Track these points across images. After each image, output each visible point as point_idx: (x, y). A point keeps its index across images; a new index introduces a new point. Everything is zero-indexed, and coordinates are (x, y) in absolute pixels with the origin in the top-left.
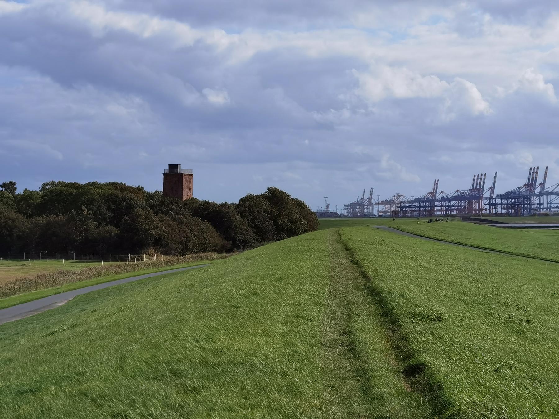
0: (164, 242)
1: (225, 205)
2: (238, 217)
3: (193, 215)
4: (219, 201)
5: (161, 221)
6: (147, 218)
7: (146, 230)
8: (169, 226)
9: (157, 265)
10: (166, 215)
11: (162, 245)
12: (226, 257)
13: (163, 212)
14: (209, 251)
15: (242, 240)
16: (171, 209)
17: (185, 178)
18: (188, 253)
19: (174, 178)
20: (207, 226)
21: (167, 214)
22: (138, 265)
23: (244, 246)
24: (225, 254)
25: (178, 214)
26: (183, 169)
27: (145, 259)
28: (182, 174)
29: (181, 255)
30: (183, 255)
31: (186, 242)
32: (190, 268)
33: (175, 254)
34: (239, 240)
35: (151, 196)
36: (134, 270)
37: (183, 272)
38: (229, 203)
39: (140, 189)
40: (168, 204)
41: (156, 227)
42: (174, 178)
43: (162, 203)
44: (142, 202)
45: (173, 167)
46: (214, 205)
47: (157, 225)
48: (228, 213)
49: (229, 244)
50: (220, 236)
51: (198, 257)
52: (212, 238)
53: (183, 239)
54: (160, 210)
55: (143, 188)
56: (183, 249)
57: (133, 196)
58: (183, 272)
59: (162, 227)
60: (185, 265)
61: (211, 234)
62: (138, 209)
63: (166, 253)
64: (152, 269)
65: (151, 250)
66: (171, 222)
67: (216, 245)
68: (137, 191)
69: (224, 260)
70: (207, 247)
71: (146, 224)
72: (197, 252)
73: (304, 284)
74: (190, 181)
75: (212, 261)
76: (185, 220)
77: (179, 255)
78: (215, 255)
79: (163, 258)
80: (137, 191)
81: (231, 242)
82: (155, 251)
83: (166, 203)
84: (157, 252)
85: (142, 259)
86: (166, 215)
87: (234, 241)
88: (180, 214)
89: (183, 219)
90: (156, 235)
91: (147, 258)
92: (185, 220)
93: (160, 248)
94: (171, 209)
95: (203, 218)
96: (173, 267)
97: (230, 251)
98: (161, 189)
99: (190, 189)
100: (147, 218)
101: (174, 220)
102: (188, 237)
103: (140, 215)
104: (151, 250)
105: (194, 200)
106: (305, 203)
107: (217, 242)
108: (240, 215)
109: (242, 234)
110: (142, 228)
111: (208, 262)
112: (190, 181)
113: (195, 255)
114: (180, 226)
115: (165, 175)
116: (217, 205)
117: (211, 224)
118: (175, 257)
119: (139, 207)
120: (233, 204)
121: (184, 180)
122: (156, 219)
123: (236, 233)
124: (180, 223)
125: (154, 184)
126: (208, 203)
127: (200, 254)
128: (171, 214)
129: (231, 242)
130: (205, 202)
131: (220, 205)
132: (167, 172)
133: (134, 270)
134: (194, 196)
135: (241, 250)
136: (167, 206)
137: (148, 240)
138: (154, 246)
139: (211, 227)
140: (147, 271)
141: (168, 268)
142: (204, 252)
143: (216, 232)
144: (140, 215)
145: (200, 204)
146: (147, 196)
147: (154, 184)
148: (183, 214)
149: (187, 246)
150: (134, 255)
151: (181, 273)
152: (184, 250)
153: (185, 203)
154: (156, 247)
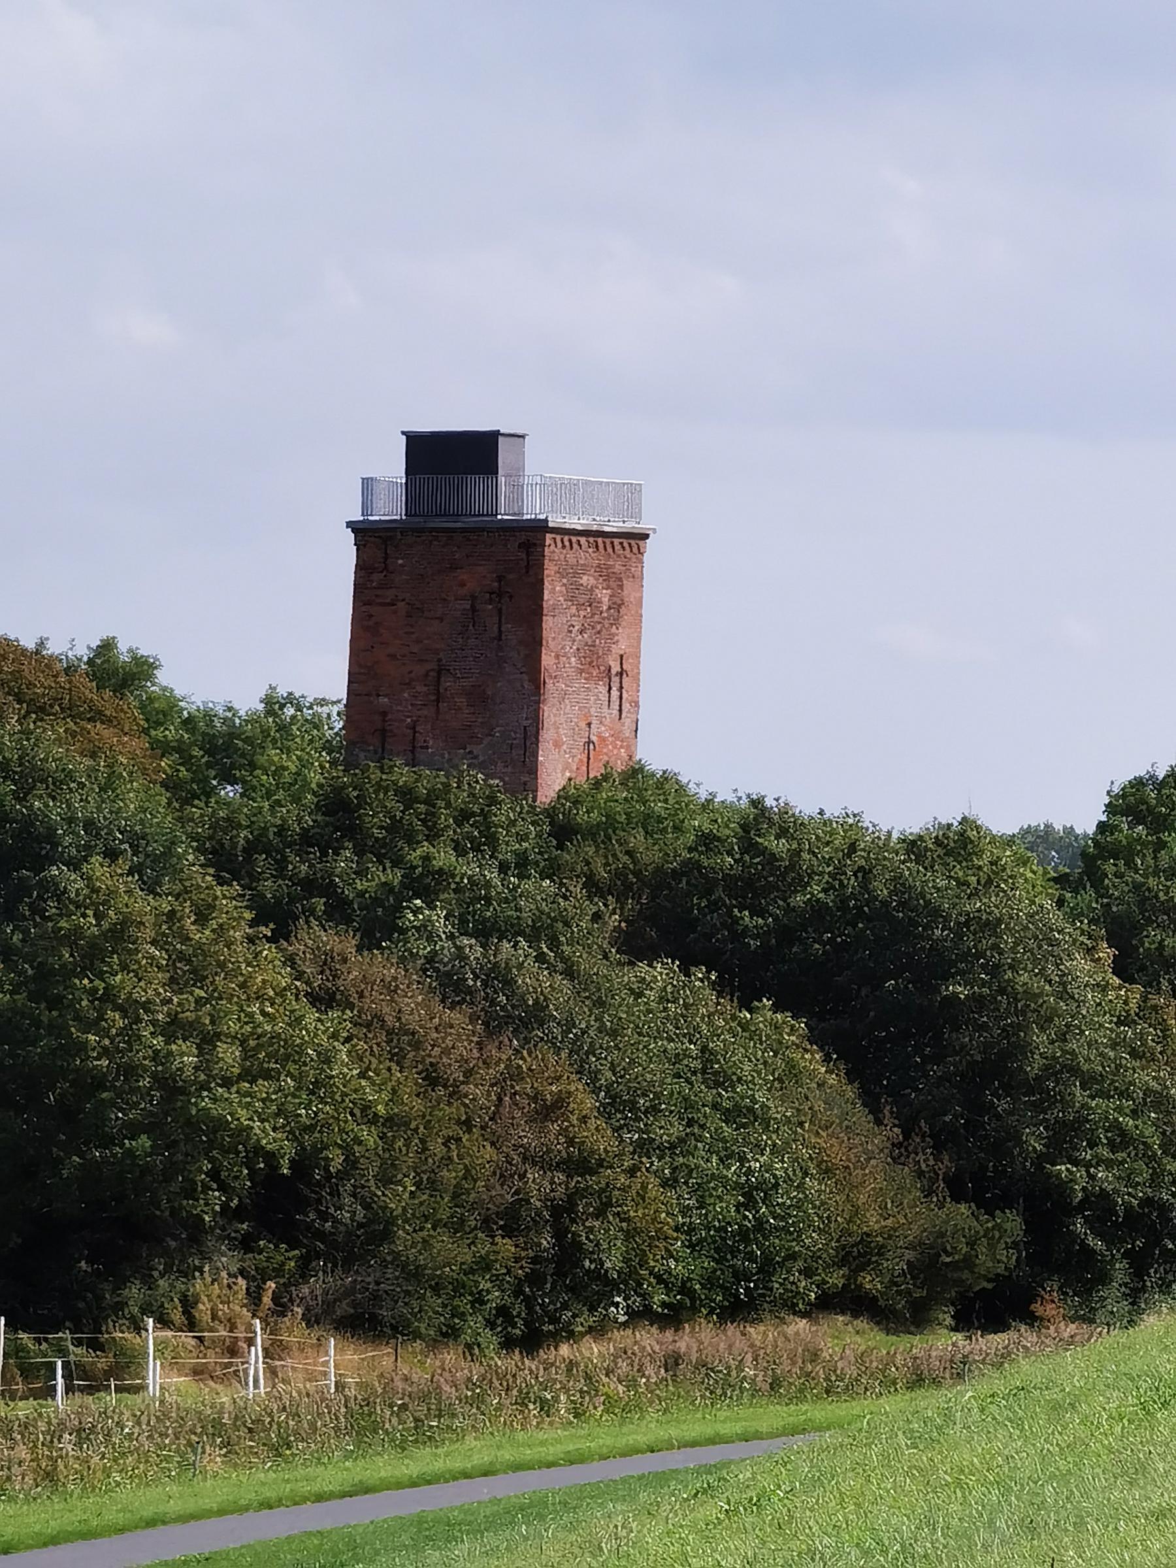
0: (349, 1212)
1: (958, 844)
2: (1089, 968)
3: (635, 946)
4: (898, 805)
5: (323, 1000)
6: (190, 969)
7: (172, 1088)
8: (400, 1043)
9: (265, 1437)
10: (369, 942)
11: (321, 1242)
12: (960, 1369)
13: (339, 912)
14: (790, 1305)
15: (1127, 1198)
16: (426, 884)
17: (572, 574)
18: (586, 1320)
19: (463, 568)
20: (774, 1053)
21: (377, 926)
22: (83, 1435)
23: (1139, 1265)
24: (943, 1342)
25: (485, 932)
26: (544, 481)
27: (155, 1375)
28: (540, 528)
29: (508, 1344)
30: (530, 1342)
31: (562, 1213)
32: (593, 1472)
33: (449, 1334)
34: (1099, 1205)
35: (218, 749)
36: (50, 1477)
37: (535, 1510)
38: (1002, 820)
39: (118, 675)
40: (394, 827)
41: (266, 1059)
42: (463, 568)
43: (339, 814)
44: (139, 802)
45: (452, 461)
46: (850, 842)
47: (265, 1028)
48: (991, 926)
49: (994, 1241)
50: (899, 1152)
51: (673, 1362)
52: (827, 1171)
53: (539, 1185)
54: (310, 886)
55: (143, 668)
56: (535, 1279)
57: (53, 745)
58: (535, 1510)
59: (326, 1059)
60: (553, 1438)
61: (808, 1130)
62: (97, 866)
63: (362, 1322)
64: (219, 1480)
65: (218, 1286)
66: (415, 1005)
67: (858, 1254)
68: (88, 689)
69: (930, 1401)
70: (767, 1267)
71: (173, 1028)
72: (672, 1318)
73: (178, 771)
74: (614, 608)
75: (818, 1412)
76: (558, 992)
77: (490, 1339)
78: (846, 1340)
79: (336, 1362)
80: (88, 689)
81: (1012, 1222)
82: (254, 1297)
83: (375, 823)
84: (281, 1306)
85: (124, 1371)
86: (369, 942)
87: (1046, 1208)
88: (511, 931)
89: (535, 980)
90: (269, 1136)
91: (173, 1363)
92: (558, 992)
93: (304, 1270)
94: (426, 884)
95: (743, 982)
96: (423, 1460)
97: (996, 1307)
98: (322, 675)
99: (617, 677)
100: (190, 969)
101: (450, 986)
102: (581, 1164)
103: (120, 934)
104: (218, 1286)
105: (647, 796)
106: (54, 648)
107: (873, 1221)
108: (1106, 953)
109: (1122, 1140)
110: (130, 1071)
111: (775, 1415)
112: (617, 606)
113: (649, 1339)
114: (503, 1052)
115: (366, 534)
116: (882, 845)
117: (816, 1037)
118: (450, 1356)
119: (112, 855)
120: (1040, 839)
121: (553, 591)
122: (270, 969)
123: (1067, 1137)
124: (513, 1018)
125: (266, 634)
126: (786, 824)
127: (700, 1339)
128: (426, 931)
129: (1012, 1222)
130: (759, 818)
131: (913, 846)
132: (390, 508)
133: (50, 1477)
134: (654, 756)
135: (1112, 1296)
136: (385, 853)
137: (190, 1192)
138: (246, 1244)
139: (812, 1061)
140: (171, 1496)
141: (383, 1465)
142: (736, 1311)
143: (861, 1117)
144: (120, 934)
145: (707, 841)
146: (180, 749)
147: (266, 634)
148: (543, 931)
149: (569, 1253)
150: (42, 1326)
151: (505, 1517)
152: (548, 1288)
153: (562, 827)
154: (270, 1251)
